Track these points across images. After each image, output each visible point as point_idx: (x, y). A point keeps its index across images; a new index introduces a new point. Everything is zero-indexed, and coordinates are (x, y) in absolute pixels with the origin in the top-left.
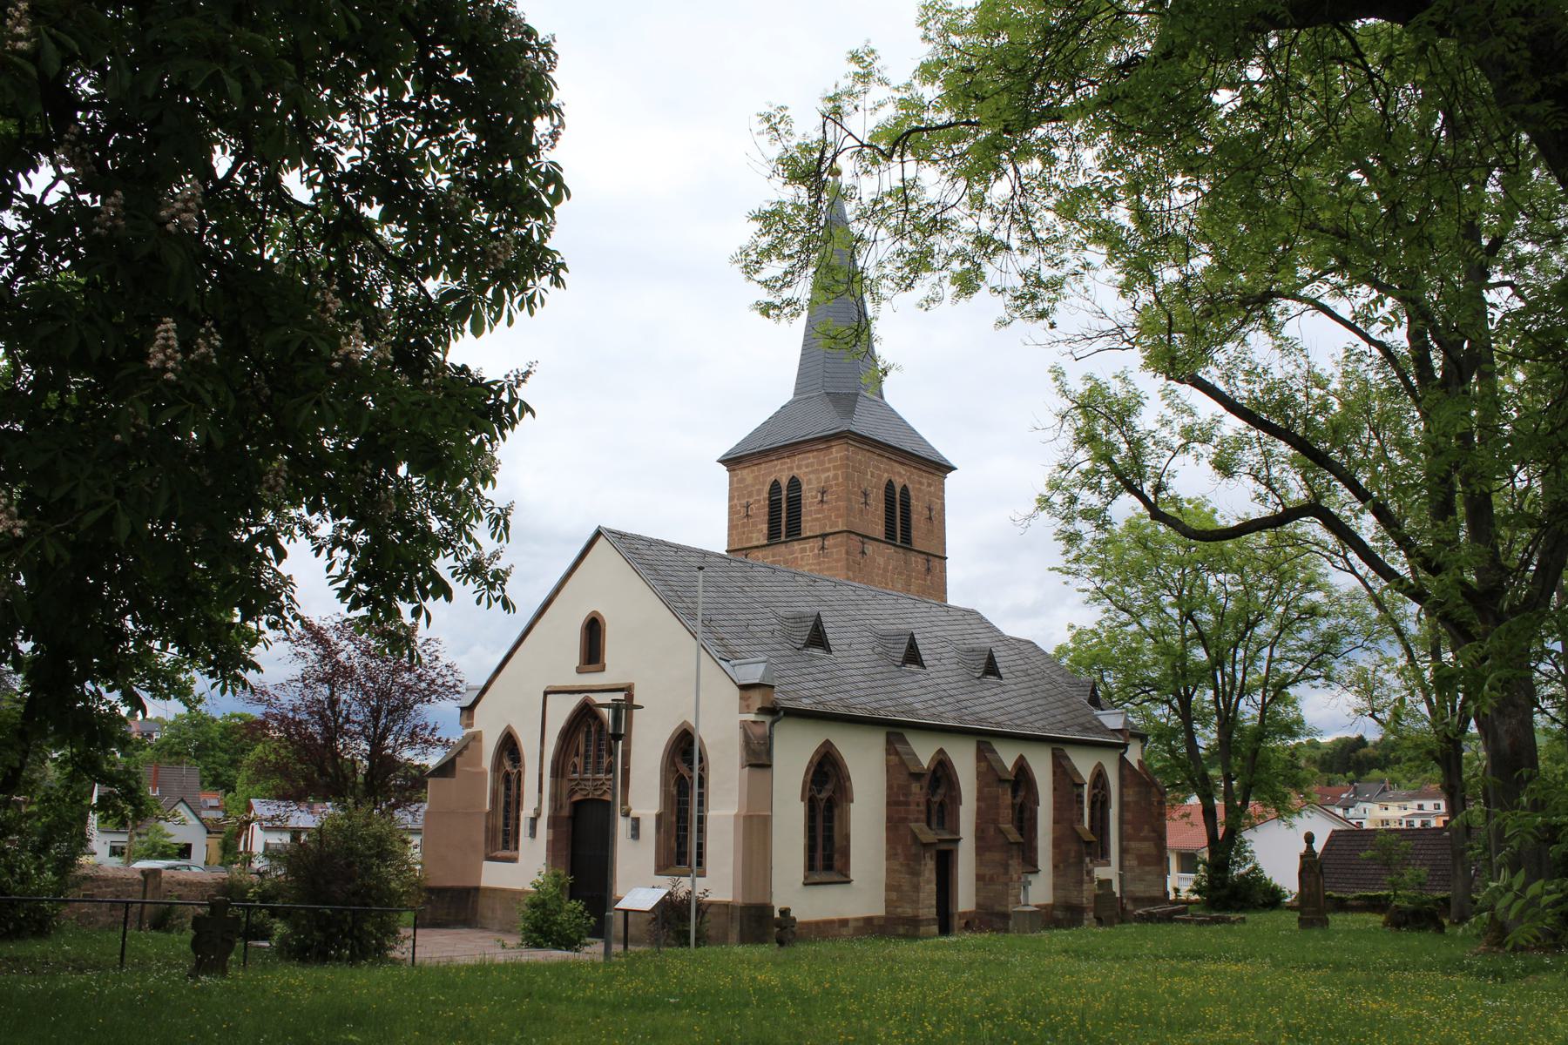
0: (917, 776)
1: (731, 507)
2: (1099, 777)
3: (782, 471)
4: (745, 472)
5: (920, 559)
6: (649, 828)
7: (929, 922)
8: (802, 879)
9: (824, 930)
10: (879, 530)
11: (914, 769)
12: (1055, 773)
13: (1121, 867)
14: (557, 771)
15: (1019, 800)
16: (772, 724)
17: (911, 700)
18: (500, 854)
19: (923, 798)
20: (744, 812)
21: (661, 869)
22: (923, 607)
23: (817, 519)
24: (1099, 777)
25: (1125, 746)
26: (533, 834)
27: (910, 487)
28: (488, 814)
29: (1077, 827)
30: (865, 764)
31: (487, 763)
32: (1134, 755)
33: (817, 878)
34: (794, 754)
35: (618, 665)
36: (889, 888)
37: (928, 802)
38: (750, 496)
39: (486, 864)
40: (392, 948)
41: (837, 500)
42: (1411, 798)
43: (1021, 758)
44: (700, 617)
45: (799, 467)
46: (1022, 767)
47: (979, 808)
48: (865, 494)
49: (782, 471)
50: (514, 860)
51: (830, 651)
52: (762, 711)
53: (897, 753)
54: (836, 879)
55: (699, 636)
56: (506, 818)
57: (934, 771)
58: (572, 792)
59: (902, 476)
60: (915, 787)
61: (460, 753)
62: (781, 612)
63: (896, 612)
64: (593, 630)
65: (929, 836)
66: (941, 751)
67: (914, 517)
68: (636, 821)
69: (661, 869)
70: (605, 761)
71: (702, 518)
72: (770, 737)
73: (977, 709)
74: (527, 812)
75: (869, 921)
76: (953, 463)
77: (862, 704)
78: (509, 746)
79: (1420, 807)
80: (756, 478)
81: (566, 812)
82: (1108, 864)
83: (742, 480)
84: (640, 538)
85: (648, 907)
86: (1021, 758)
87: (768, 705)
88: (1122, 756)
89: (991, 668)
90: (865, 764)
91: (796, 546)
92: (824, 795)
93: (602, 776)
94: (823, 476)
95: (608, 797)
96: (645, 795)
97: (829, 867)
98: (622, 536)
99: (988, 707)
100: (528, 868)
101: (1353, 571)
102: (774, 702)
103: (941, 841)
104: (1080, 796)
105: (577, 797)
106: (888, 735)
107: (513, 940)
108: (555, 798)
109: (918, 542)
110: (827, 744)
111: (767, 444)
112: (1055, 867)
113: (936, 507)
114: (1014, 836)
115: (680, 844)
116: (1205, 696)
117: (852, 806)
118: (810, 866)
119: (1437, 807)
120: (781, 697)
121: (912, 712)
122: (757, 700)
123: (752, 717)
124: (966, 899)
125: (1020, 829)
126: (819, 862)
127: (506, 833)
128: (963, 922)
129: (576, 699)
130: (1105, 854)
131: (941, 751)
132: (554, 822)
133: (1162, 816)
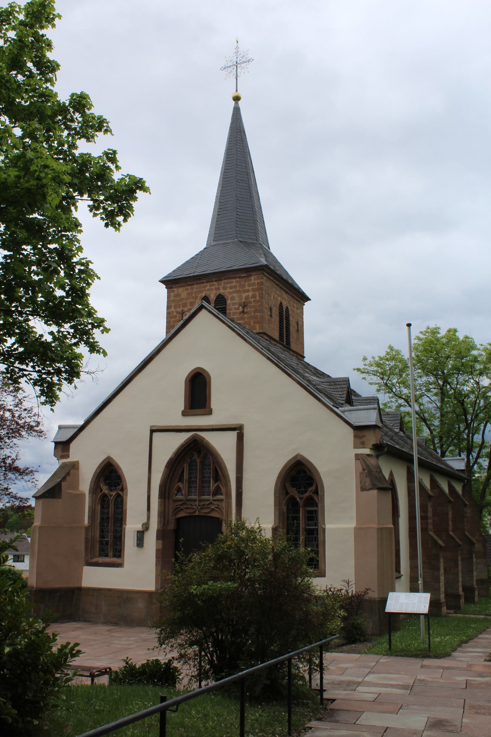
1: (168, 314)
4: (180, 290)
10: (276, 335)
18: (95, 560)
26: (140, 542)
27: (289, 308)
28: (87, 528)
35: (223, 406)
38: (185, 305)
41: (255, 312)
45: (225, 288)
48: (271, 310)
56: (102, 531)
58: (177, 510)
59: (287, 301)
61: (64, 479)
67: (291, 328)
74: (132, 525)
78: (109, 475)
80: (189, 294)
81: (172, 526)
83: (178, 295)
94: (244, 295)
105: (181, 515)
107: (152, 635)
108: (163, 515)
109: (293, 346)
111: (198, 272)
113: (300, 323)
122: (372, 438)
123: (367, 451)
129: (184, 437)
132: (161, 535)
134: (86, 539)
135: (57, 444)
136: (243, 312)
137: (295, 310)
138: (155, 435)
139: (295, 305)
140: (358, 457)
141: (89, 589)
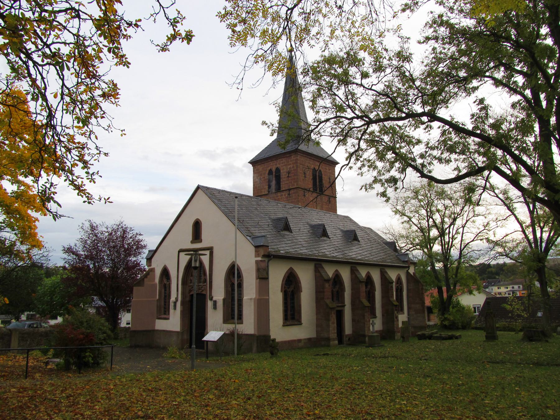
0: (328, 281)
2: (399, 279)
3: (273, 166)
4: (259, 166)
5: (327, 198)
6: (220, 304)
7: (334, 340)
8: (282, 324)
9: (292, 346)
10: (310, 186)
11: (326, 278)
12: (381, 279)
13: (408, 315)
14: (184, 282)
15: (368, 289)
16: (268, 261)
17: (325, 251)
19: (329, 291)
20: (258, 297)
21: (226, 321)
22: (328, 215)
23: (287, 183)
24: (399, 279)
25: (409, 267)
26: (175, 308)
28: (157, 300)
29: (391, 299)
30: (306, 277)
31: (157, 280)
32: (412, 270)
33: (288, 323)
34: (277, 275)
35: (207, 240)
36: (317, 326)
37: (332, 291)
39: (157, 320)
40: (103, 363)
42: (509, 285)
43: (368, 273)
44: (236, 217)
46: (369, 277)
47: (352, 293)
49: (273, 166)
50: (168, 319)
51: (292, 232)
52: (264, 256)
53: (319, 272)
54: (296, 323)
55: (236, 224)
56: (165, 302)
57: (334, 279)
60: (327, 285)
62: (272, 217)
63: (316, 217)
64: (197, 226)
65: (334, 305)
66: (337, 271)
67: (324, 182)
68: (215, 303)
69: (226, 321)
70: (203, 278)
71: (243, 182)
72: (268, 266)
73: (350, 254)
74: (173, 299)
75: (309, 339)
76: (338, 161)
77: (304, 251)
78: (165, 273)
79: (513, 288)
81: (188, 299)
82: (404, 314)
84: (215, 189)
85: (216, 339)
86: (368, 273)
87: (266, 254)
88: (407, 271)
89: (356, 238)
90: (306, 277)
91: (279, 194)
92: (291, 289)
93: (201, 284)
95: (204, 293)
96: (219, 292)
97: (293, 318)
98: (208, 188)
99: (355, 253)
100: (173, 322)
101: (497, 197)
102: (269, 252)
103: (338, 306)
104: (392, 287)
106: (315, 265)
110: (291, 269)
111: (267, 156)
112: (383, 315)
114: (366, 303)
115: (233, 312)
116: (437, 248)
117: (302, 294)
118: (286, 318)
119: (519, 287)
120: (271, 249)
121: (325, 256)
122: (262, 251)
123: (260, 259)
124: (348, 329)
125: (369, 301)
126: (289, 317)
127: (165, 308)
128: (347, 339)
130: (402, 310)
131: (337, 271)
132: (183, 304)
133: (423, 294)
134: (157, 306)
135: (147, 259)
136: (288, 177)
137: (327, 171)
138: (181, 253)
139: (327, 168)
140: (256, 261)
141: (158, 330)
